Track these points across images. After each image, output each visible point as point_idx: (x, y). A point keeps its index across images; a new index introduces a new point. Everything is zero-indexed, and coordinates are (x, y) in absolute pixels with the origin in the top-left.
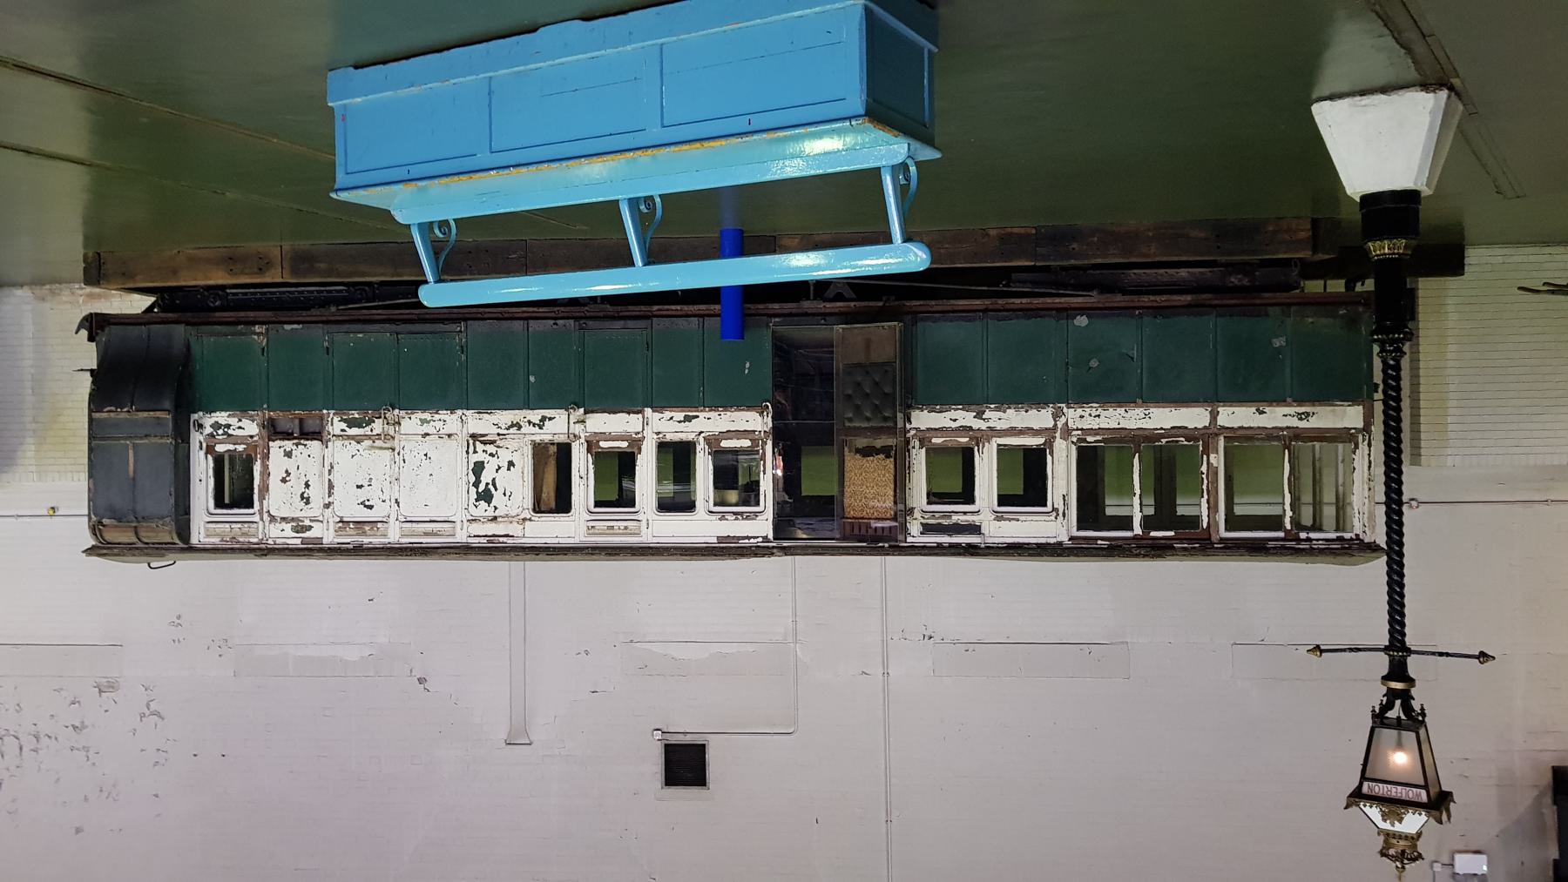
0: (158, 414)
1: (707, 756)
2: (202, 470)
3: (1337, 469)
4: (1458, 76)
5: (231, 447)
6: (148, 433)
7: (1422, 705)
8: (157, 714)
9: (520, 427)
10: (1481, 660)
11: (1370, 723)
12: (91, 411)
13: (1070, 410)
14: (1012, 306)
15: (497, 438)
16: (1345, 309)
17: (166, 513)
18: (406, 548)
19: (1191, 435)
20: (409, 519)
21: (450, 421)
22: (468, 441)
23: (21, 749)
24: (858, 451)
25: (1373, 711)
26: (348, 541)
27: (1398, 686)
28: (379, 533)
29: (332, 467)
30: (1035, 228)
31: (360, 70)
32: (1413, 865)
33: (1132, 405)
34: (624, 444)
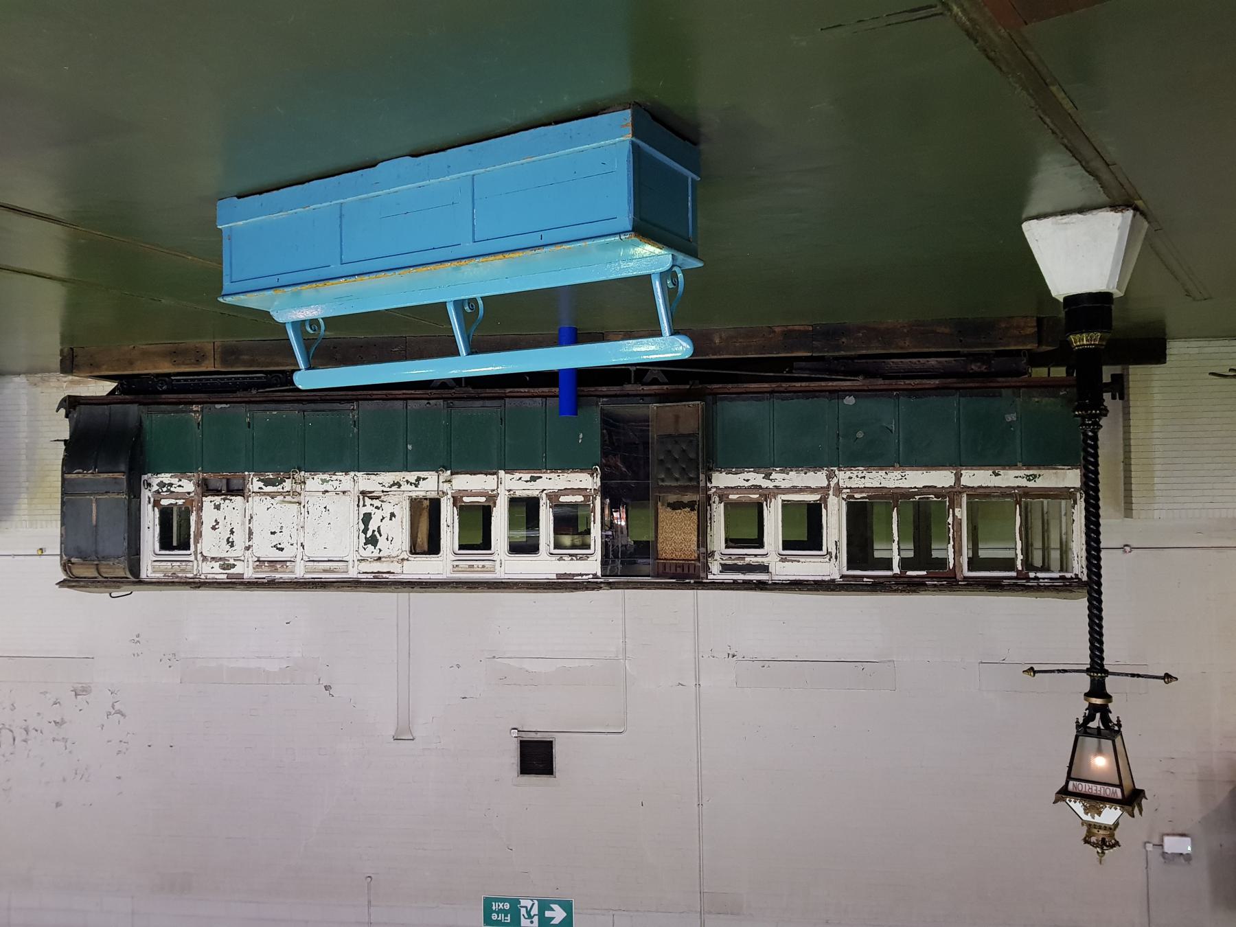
0: (116, 475)
1: (554, 751)
2: (150, 520)
3: (1061, 521)
4: (1141, 199)
5: (173, 501)
6: (107, 491)
7: (1118, 717)
8: (119, 712)
9: (400, 486)
10: (1166, 680)
11: (1074, 732)
12: (63, 473)
13: (841, 472)
14: (794, 389)
15: (381, 494)
16: (1065, 391)
17: (121, 553)
18: (309, 582)
19: (940, 493)
20: (311, 559)
21: (345, 481)
22: (358, 497)
23: (14, 740)
24: (669, 505)
25: (1077, 722)
26: (264, 576)
27: (1098, 701)
28: (288, 570)
29: (252, 518)
30: (812, 326)
31: (242, 199)
32: (1111, 850)
33: (891, 468)
34: (483, 499)
